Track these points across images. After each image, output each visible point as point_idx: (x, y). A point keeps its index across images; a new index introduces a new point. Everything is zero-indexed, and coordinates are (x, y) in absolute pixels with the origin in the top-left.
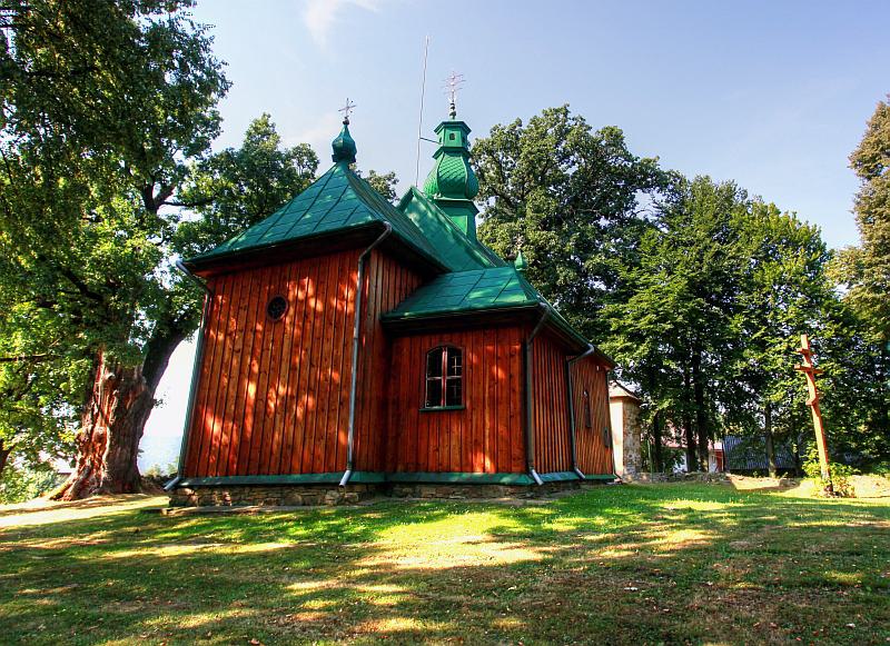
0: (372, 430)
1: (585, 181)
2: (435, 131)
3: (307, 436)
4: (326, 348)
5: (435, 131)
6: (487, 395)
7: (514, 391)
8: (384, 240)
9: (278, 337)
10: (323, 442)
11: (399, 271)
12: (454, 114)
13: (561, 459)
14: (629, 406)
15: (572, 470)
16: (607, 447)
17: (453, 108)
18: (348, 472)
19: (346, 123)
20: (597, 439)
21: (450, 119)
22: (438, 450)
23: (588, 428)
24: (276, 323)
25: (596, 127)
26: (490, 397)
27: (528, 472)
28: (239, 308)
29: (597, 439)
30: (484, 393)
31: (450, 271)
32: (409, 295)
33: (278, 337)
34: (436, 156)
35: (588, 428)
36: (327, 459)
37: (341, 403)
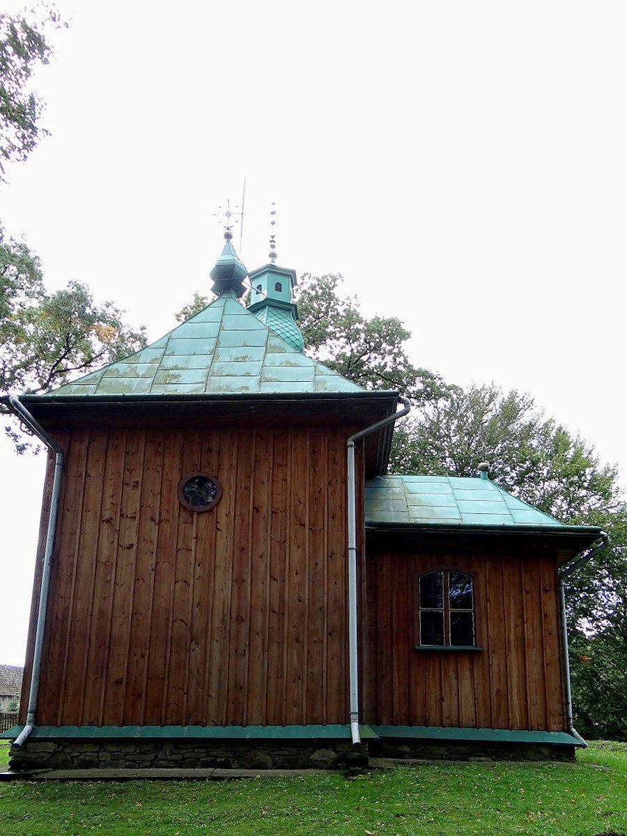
17: (273, 247)
19: (228, 236)
22: (442, 699)
24: (199, 513)
26: (517, 638)
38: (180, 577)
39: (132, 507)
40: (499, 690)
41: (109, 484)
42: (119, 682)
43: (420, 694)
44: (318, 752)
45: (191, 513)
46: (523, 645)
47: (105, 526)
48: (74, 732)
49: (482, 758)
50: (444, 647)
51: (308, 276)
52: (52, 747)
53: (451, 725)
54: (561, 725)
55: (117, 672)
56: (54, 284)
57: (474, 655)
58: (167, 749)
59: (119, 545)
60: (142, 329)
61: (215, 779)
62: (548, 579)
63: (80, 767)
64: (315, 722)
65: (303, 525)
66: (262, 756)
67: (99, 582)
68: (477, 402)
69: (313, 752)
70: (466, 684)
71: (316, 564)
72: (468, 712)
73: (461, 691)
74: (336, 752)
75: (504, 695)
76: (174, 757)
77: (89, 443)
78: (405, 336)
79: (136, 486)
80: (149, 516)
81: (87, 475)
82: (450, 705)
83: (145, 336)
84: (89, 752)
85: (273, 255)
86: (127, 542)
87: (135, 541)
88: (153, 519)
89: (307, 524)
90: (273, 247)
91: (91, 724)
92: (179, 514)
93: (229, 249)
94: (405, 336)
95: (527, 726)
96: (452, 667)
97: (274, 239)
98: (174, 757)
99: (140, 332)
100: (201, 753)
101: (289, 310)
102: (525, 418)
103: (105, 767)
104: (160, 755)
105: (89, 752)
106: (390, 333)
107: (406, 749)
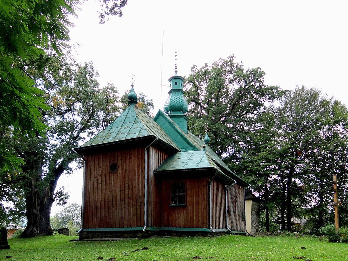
0: (153, 212)
1: (241, 93)
2: (169, 80)
3: (129, 215)
4: (134, 183)
5: (169, 80)
6: (194, 201)
7: (205, 200)
8: (155, 143)
9: (115, 178)
10: (135, 217)
11: (159, 152)
12: (176, 72)
13: (222, 224)
14: (254, 203)
15: (226, 227)
16: (243, 220)
17: (176, 68)
18: (145, 227)
19: (132, 86)
20: (238, 216)
21: (174, 75)
22: (176, 220)
23: (235, 212)
24: (114, 173)
25: (247, 67)
26: (196, 201)
27: (209, 228)
28: (98, 167)
29: (238, 216)
30: (194, 200)
31: (179, 151)
32: (165, 162)
33: (115, 178)
34: (170, 93)
35: (235, 212)
36: (137, 222)
37: (141, 203)
38: (110, 190)
39: (100, 173)
40: (190, 217)
41: (95, 167)
42: (98, 218)
43: (171, 219)
44: (139, 234)
45: (116, 173)
46: (197, 203)
47: (95, 178)
48: (90, 230)
49: (184, 236)
50: (177, 205)
51: (221, 59)
52: (86, 233)
53: (179, 227)
54: (206, 226)
55: (98, 215)
56: (121, 94)
57: (185, 207)
58: (108, 234)
59: (98, 183)
60: (151, 100)
61: (113, 240)
62: (205, 183)
63: (91, 238)
64: (138, 226)
65: (136, 174)
66: (126, 235)
67: (94, 193)
68: (299, 93)
69: (137, 234)
70: (182, 215)
71: (139, 185)
72: (183, 223)
73: (181, 218)
74: (142, 234)
75: (192, 218)
76: (109, 236)
77: (91, 157)
78: (262, 74)
79: (101, 168)
80: (103, 175)
81: (91, 166)
82: (178, 221)
83: (153, 103)
84: (93, 234)
85: (176, 72)
86: (99, 183)
87: (101, 182)
88: (104, 176)
89: (136, 174)
90: (176, 68)
91: (94, 228)
92: (110, 174)
93: (133, 90)
94: (262, 74)
95: (197, 227)
96: (179, 211)
97: (176, 66)
98: (109, 236)
99: (150, 102)
100: (114, 235)
101: (180, 91)
102: (320, 98)
103: (96, 238)
104: (107, 235)
105: (93, 234)
106: (257, 74)
107: (166, 233)
